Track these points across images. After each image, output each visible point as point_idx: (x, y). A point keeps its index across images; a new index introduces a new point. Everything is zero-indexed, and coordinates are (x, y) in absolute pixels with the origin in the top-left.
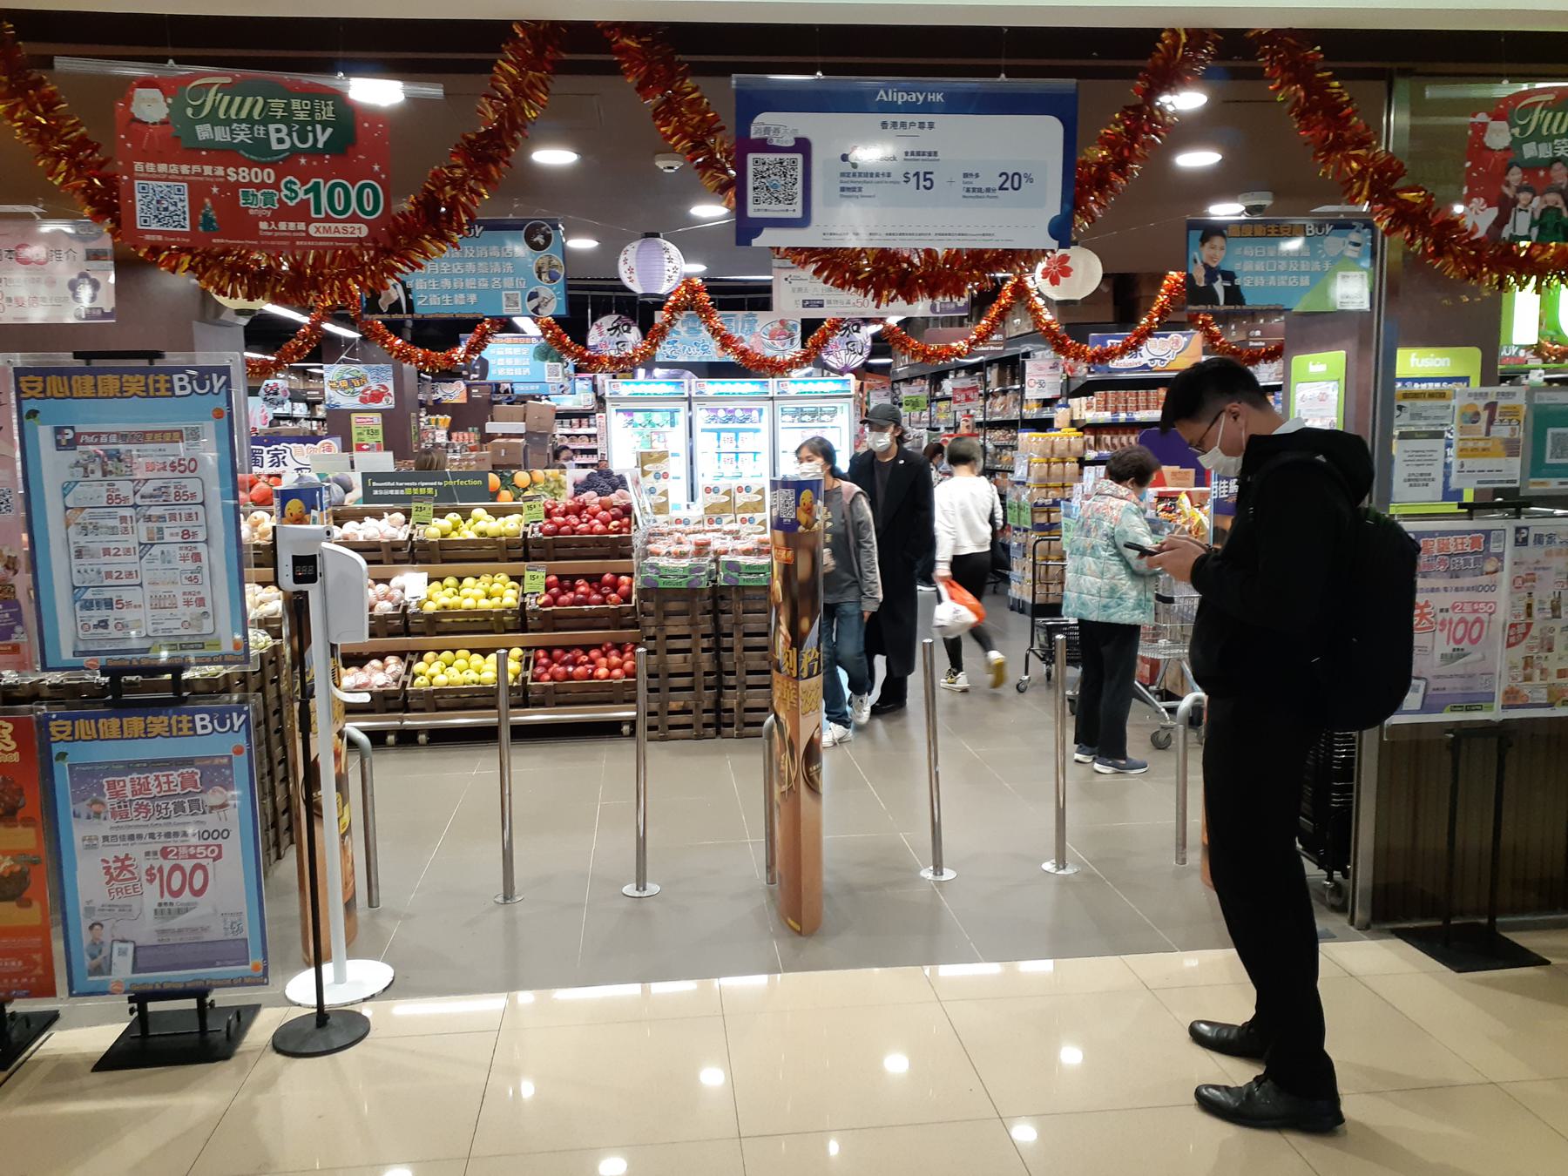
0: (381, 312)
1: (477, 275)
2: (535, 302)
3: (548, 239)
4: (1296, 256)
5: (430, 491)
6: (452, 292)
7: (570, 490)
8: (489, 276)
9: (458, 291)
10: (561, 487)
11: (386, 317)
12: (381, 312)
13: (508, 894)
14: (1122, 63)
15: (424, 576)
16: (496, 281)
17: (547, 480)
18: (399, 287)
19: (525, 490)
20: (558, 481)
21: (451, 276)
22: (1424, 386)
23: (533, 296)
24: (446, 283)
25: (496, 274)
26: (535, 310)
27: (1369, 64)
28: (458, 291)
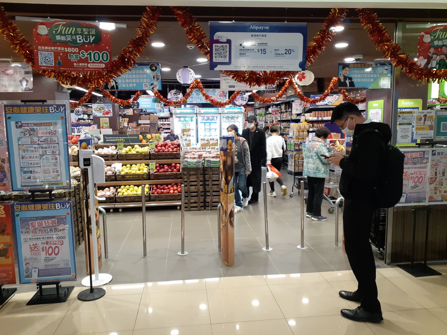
0: (109, 89)
1: (136, 78)
2: (152, 86)
3: (156, 68)
4: (369, 73)
5: (123, 140)
6: (129, 83)
7: (163, 139)
8: (139, 79)
9: (131, 83)
10: (160, 139)
11: (110, 90)
12: (109, 89)
13: (145, 255)
14: (320, 18)
15: (121, 164)
16: (141, 80)
17: (156, 137)
18: (114, 82)
19: (150, 139)
20: (159, 137)
21: (129, 79)
22: (406, 110)
23: (152, 84)
24: (127, 81)
25: (142, 78)
26: (153, 88)
27: (390, 18)
28: (131, 83)
